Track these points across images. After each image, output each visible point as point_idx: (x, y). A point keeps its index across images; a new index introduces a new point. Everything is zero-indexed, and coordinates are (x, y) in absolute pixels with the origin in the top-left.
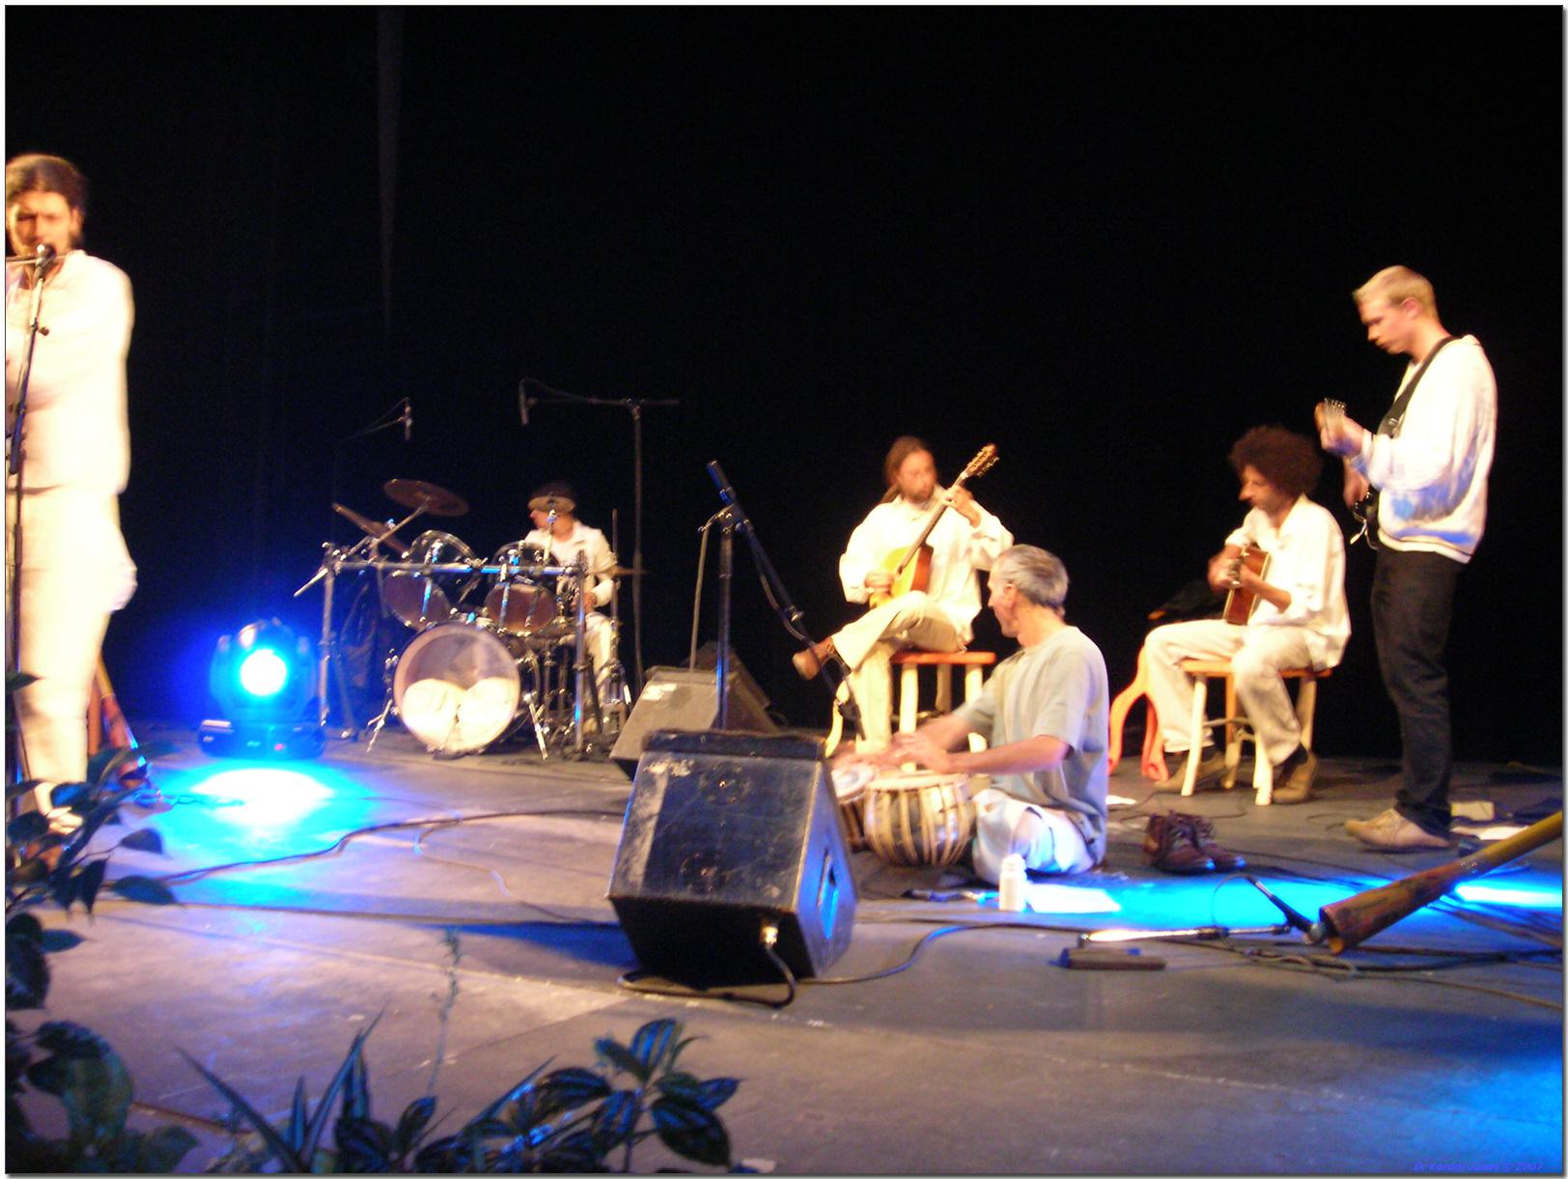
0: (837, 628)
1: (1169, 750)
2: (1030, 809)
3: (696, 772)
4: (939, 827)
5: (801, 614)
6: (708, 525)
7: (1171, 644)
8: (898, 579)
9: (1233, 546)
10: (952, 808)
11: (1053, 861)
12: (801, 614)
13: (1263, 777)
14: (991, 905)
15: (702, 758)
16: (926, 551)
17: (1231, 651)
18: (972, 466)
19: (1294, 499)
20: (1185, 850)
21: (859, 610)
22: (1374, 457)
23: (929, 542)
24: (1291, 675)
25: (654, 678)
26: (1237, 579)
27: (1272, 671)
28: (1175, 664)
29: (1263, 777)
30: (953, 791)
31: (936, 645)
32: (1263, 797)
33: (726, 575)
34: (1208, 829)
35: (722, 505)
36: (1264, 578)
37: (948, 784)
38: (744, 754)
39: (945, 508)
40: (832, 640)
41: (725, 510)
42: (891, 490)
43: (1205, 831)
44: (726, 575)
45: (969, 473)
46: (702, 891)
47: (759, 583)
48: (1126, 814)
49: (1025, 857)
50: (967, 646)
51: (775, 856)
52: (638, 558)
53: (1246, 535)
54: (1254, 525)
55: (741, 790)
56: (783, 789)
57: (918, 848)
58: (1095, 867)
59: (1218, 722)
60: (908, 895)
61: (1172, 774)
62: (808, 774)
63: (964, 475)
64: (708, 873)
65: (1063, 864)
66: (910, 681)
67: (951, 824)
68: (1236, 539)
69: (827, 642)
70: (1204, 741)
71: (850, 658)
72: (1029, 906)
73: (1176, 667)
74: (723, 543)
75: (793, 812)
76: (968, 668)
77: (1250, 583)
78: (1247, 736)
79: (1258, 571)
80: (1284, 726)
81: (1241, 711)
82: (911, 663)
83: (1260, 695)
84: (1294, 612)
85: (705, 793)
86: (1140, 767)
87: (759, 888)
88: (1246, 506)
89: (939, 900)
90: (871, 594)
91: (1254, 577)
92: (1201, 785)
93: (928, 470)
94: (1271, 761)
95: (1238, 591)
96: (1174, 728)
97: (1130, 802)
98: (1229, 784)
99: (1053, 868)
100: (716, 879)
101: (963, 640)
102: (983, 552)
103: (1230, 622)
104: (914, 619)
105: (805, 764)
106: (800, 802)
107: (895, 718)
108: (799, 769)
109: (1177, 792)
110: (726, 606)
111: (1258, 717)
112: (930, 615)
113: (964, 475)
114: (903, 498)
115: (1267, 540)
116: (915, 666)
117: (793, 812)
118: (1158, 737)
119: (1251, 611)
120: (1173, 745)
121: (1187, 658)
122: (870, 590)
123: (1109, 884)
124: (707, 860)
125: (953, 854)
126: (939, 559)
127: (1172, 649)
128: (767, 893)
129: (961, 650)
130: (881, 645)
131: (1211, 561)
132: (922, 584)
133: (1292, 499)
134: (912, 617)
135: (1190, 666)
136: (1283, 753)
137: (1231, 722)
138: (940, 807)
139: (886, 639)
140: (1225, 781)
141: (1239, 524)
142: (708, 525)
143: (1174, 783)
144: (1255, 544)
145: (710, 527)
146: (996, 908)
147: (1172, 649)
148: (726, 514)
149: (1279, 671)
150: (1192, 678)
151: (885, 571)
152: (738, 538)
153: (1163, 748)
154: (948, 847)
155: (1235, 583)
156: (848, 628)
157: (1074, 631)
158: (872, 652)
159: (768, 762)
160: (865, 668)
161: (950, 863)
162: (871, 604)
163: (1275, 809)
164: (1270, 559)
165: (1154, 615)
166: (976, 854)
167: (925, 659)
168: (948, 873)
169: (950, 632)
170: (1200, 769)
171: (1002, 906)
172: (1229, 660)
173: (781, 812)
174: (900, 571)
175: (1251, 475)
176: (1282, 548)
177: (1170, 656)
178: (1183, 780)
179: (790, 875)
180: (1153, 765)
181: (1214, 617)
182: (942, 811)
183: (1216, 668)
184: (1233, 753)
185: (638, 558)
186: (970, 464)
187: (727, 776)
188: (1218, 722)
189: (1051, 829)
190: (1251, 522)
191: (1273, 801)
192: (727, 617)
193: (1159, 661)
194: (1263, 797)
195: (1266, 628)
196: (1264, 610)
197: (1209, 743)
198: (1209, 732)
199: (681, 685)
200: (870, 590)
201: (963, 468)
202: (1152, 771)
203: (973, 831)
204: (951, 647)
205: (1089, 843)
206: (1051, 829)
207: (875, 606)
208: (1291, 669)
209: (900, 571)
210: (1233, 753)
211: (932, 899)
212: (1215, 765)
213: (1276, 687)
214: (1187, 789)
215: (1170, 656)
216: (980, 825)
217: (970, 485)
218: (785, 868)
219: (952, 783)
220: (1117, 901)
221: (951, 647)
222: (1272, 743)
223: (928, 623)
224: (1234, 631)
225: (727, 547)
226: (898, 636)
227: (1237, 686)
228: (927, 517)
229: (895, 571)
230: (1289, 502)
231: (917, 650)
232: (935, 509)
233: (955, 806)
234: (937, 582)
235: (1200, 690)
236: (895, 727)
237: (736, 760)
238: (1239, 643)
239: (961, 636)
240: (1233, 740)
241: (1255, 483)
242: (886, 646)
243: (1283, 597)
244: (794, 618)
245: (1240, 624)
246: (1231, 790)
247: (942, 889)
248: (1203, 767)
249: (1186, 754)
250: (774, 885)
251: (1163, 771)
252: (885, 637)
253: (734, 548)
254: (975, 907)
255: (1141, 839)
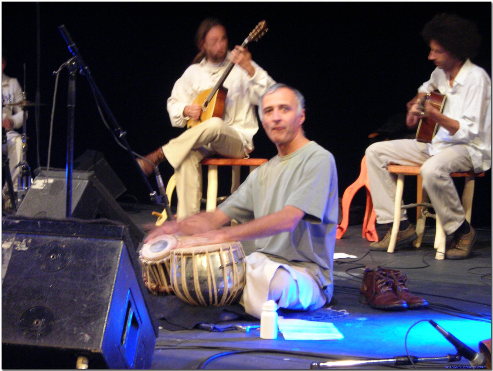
0: (166, 142)
1: (379, 222)
2: (281, 267)
3: (32, 248)
4: (220, 279)
5: (125, 132)
6: (60, 69)
7: (381, 154)
8: (205, 110)
9: (422, 93)
10: (228, 265)
11: (298, 302)
12: (125, 132)
13: (440, 242)
14: (255, 333)
15: (37, 238)
16: (222, 91)
17: (420, 159)
18: (252, 35)
19: (462, 63)
20: (387, 294)
21: (178, 131)
22: (202, 331)
23: (226, 84)
24: (459, 175)
25: (39, 174)
26: (423, 111)
27: (446, 175)
28: (383, 167)
29: (440, 242)
30: (229, 253)
31: (230, 153)
32: (439, 256)
33: (71, 105)
34: (404, 280)
35: (70, 56)
36: (442, 112)
37: (224, 250)
38: (68, 234)
39: (233, 65)
40: (162, 150)
41: (71, 59)
42: (200, 55)
43: (401, 281)
44: (71, 105)
45: (249, 39)
46: (33, 337)
47: (97, 109)
48: (351, 266)
49: (277, 302)
50: (249, 154)
51: (89, 311)
52: (38, 95)
53: (431, 85)
54: (436, 77)
55: (66, 261)
56: (96, 260)
57: (205, 293)
58: (327, 305)
59: (412, 205)
60: (197, 327)
61: (381, 239)
62: (113, 250)
63: (246, 41)
64: (38, 323)
65: (305, 303)
66: (213, 177)
67: (226, 278)
68: (425, 88)
69: (159, 151)
70: (401, 217)
71: (173, 161)
72: (280, 335)
73: (385, 169)
74: (70, 82)
75: (101, 278)
76: (251, 168)
77: (432, 114)
78: (430, 215)
79: (438, 108)
80: (454, 210)
81: (426, 198)
82: (214, 165)
83: (438, 190)
84: (461, 134)
85: (39, 262)
86: (361, 232)
87: (76, 334)
88: (432, 66)
89: (219, 331)
90: (188, 121)
91: (435, 111)
92: (399, 245)
93: (224, 38)
94: (446, 233)
95: (425, 120)
96: (383, 208)
97: (354, 257)
98: (418, 245)
99: (299, 307)
100: (44, 327)
101: (248, 149)
102: (256, 93)
103: (419, 141)
104: (214, 135)
105: (112, 243)
106: (108, 270)
107: (203, 200)
108: (107, 246)
109: (385, 250)
110: (72, 126)
111: (436, 202)
112: (225, 133)
113: (246, 41)
114: (206, 59)
115: (444, 89)
116: (216, 167)
117: (101, 278)
118: (372, 213)
119: (434, 133)
120: (381, 220)
121: (392, 164)
122: (187, 118)
123: (336, 320)
124: (40, 313)
125: (229, 298)
126: (232, 94)
127: (382, 157)
128: (81, 339)
129: (246, 157)
130: (193, 152)
131: (408, 104)
132: (221, 113)
133: (461, 62)
134: (213, 134)
135: (394, 169)
136: (453, 227)
137: (420, 205)
138: (220, 265)
139: (197, 148)
140: (416, 243)
141: (427, 78)
142: (60, 69)
143: (382, 244)
144: (437, 91)
145: (60, 72)
146: (258, 336)
147: (382, 157)
148: (72, 62)
149: (451, 175)
150: (395, 176)
151: (197, 106)
152: (79, 79)
153: (376, 221)
154: (226, 293)
155: (422, 113)
156: (172, 142)
157: (313, 143)
158: (187, 157)
159: (85, 241)
160: (183, 168)
161: (228, 303)
162: (188, 126)
163: (448, 261)
164: (446, 99)
165: (372, 136)
166: (245, 296)
167: (222, 162)
168: (226, 311)
169: (238, 143)
170: (399, 235)
171: (263, 335)
172: (420, 165)
173: (94, 277)
174: (206, 105)
175: (434, 46)
176: (453, 93)
177: (381, 162)
178: (389, 243)
179: (99, 324)
180: (369, 232)
181: (409, 138)
182: (222, 268)
183: (411, 170)
184: (421, 226)
185: (38, 95)
186: (251, 34)
187: (55, 251)
188: (412, 205)
189: (296, 281)
190: (434, 76)
191: (446, 257)
192: (72, 135)
193: (373, 165)
194: (439, 256)
195: (441, 145)
196: (443, 133)
197: (404, 219)
198: (405, 212)
199: (57, 179)
200: (187, 118)
201: (246, 36)
202: (368, 235)
203: (243, 281)
204: (240, 154)
205: (323, 289)
206: (296, 281)
207: (190, 127)
208: (460, 172)
209: (206, 105)
210: (421, 226)
211: (215, 329)
212: (409, 233)
213: (449, 184)
214: (391, 249)
215: (381, 162)
216: (248, 278)
217: (250, 48)
218: (96, 319)
219: (229, 249)
220: (341, 331)
221: (240, 154)
222: (446, 221)
223: (223, 138)
224: (422, 146)
225: (72, 85)
226: (205, 146)
227: (424, 183)
228: (221, 72)
229: (203, 104)
230: (459, 63)
231: (218, 156)
232: (228, 65)
233: (231, 265)
234: (231, 112)
235: (400, 184)
236: (203, 206)
237: (63, 239)
238: (426, 155)
239: (246, 147)
240: (421, 217)
241: (437, 51)
242: (197, 152)
243: (454, 125)
244: (121, 135)
245: (426, 142)
246: (419, 249)
247: (221, 322)
248: (401, 233)
249: (391, 225)
250: (86, 332)
251: (376, 237)
252: (196, 147)
253: (77, 86)
254: (243, 335)
255: (359, 284)
